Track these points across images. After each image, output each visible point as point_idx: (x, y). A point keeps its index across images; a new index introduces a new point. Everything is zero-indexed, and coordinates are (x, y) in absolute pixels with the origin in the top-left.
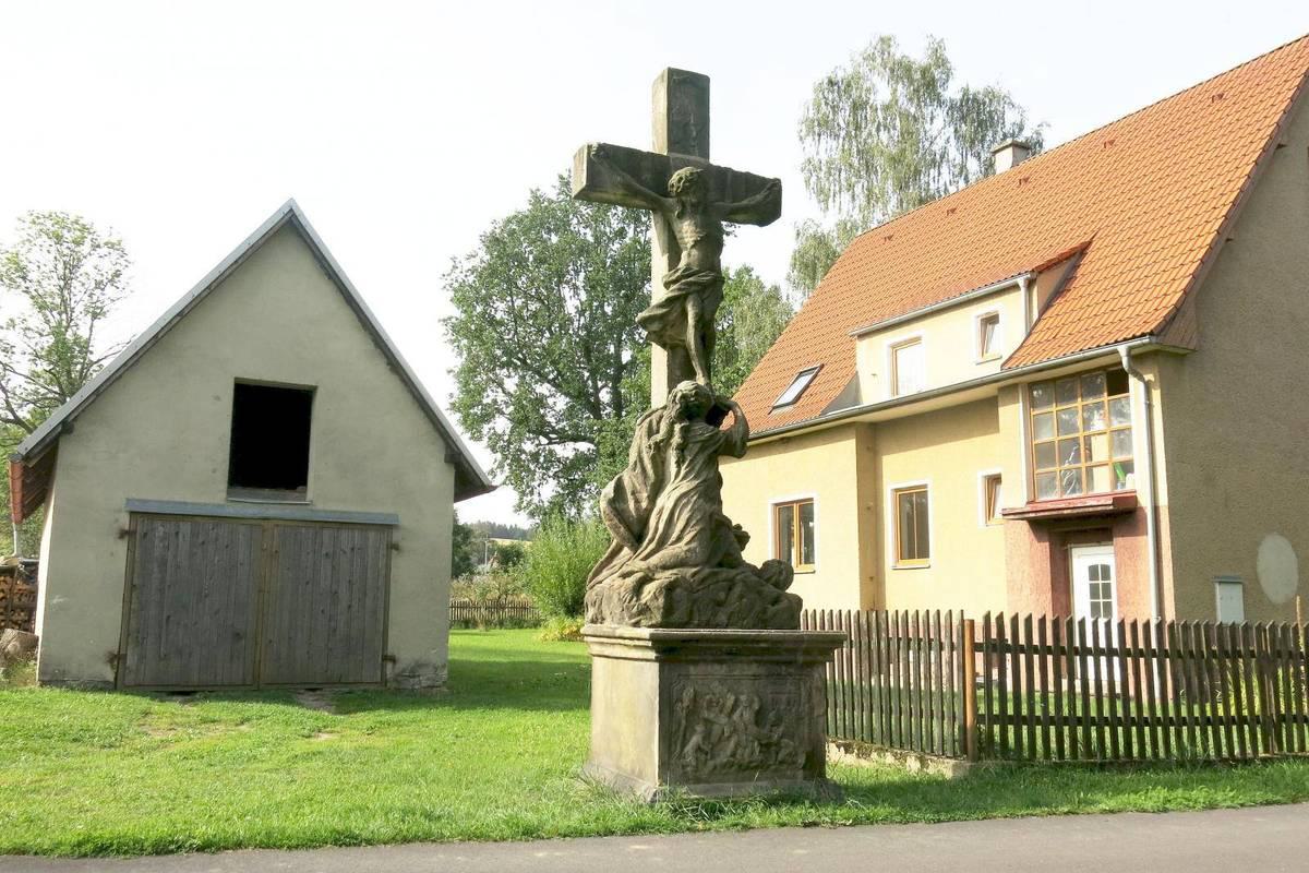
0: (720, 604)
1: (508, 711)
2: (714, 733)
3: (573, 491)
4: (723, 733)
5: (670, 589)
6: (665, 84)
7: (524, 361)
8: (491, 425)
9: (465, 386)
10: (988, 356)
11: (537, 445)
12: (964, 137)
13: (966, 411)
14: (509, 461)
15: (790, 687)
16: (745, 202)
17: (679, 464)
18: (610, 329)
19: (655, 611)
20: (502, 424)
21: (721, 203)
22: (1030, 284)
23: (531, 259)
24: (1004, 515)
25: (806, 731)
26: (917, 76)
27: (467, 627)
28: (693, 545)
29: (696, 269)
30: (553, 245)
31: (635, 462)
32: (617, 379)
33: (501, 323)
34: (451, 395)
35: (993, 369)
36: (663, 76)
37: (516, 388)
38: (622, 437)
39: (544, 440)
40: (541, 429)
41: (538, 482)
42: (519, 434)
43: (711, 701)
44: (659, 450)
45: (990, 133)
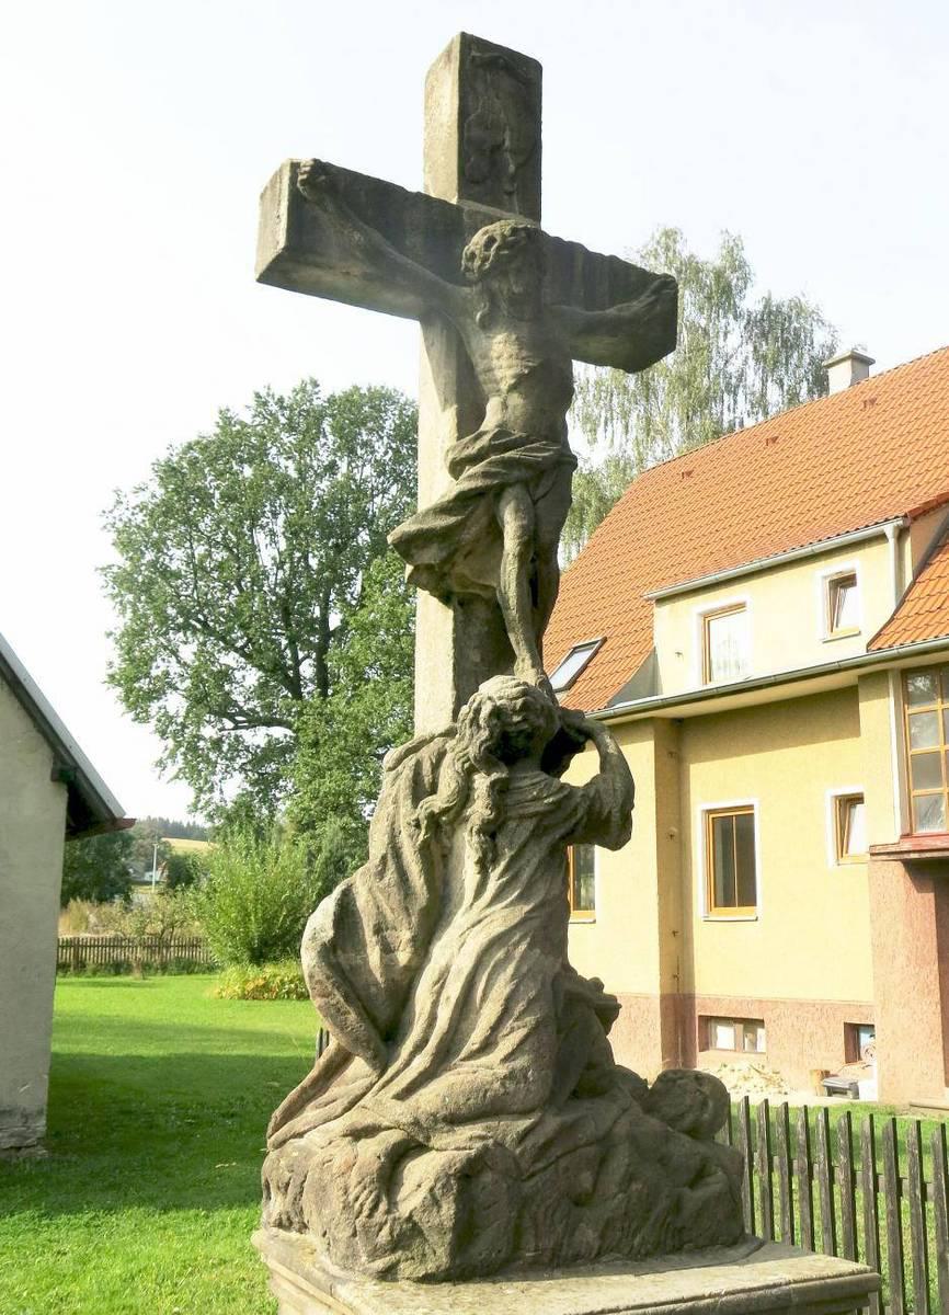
0: (579, 1201)
1: (138, 1211)
3: (265, 785)
5: (466, 1176)
6: (455, 65)
7: (205, 624)
8: (161, 703)
9: (128, 654)
10: (840, 630)
11: (221, 730)
12: (764, 357)
13: (813, 704)
14: (183, 749)
16: (612, 311)
17: (484, 865)
18: (315, 586)
19: (433, 1238)
20: (175, 703)
21: (564, 307)
22: (902, 534)
23: (217, 495)
24: (872, 854)
26: (709, 280)
27: (117, 973)
28: (521, 1062)
29: (517, 434)
30: (245, 479)
31: (384, 858)
32: (322, 650)
33: (177, 575)
34: (111, 664)
35: (855, 650)
36: (449, 53)
37: (193, 657)
38: (327, 723)
39: (229, 724)
40: (225, 709)
41: (220, 776)
42: (197, 716)
44: (439, 830)
45: (795, 355)
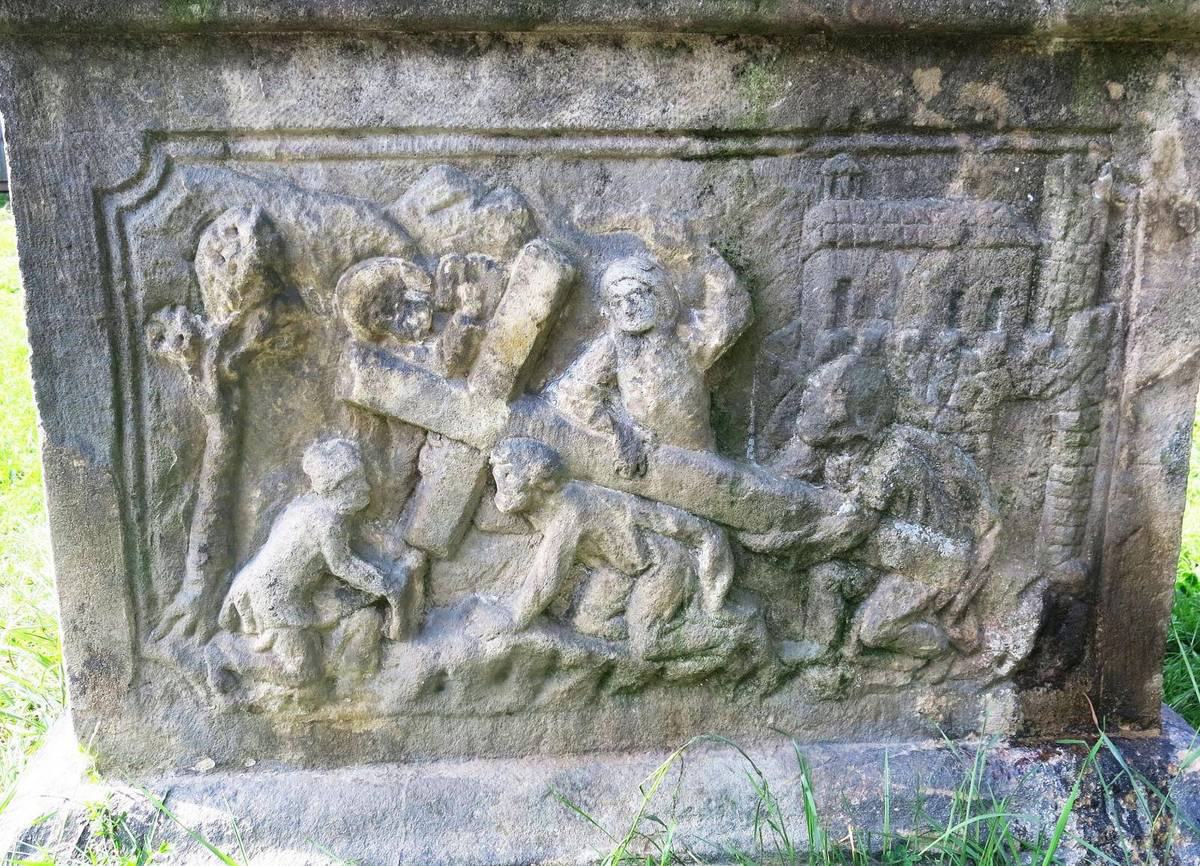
2: (430, 490)
4: (487, 483)
15: (964, 202)
25: (1060, 468)
43: (385, 303)
